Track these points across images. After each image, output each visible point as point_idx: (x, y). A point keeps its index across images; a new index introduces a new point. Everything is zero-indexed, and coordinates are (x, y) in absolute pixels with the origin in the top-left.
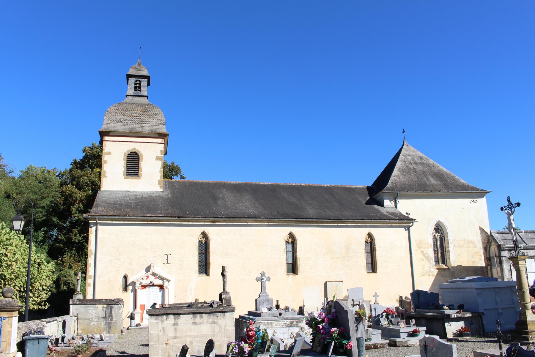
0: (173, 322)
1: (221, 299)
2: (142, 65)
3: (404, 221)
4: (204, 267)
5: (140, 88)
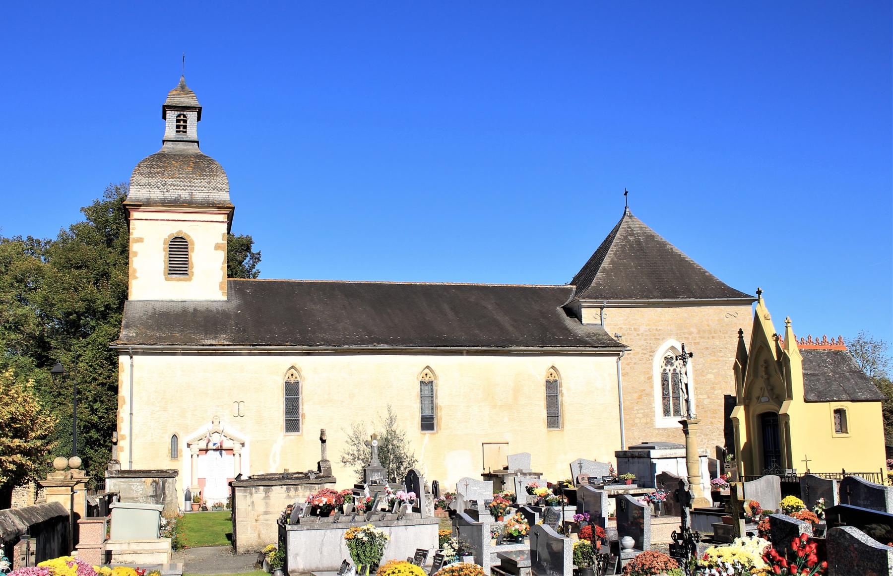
0: (264, 495)
1: (319, 467)
2: (187, 88)
3: (606, 346)
4: (293, 424)
5: (185, 127)
